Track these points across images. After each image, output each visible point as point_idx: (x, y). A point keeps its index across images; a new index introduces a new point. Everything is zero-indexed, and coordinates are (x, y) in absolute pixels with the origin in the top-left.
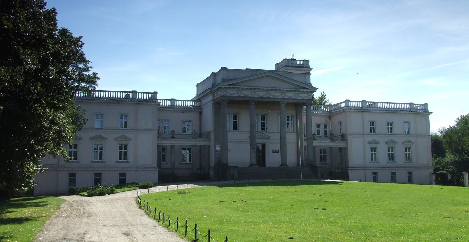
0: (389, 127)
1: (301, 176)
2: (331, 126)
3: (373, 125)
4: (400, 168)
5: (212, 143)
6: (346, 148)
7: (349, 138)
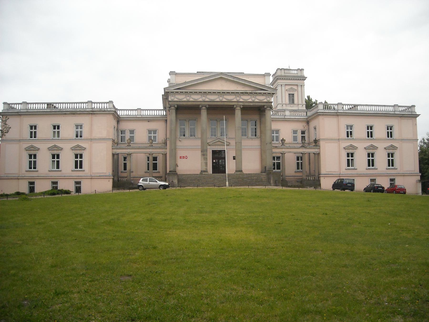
0: (389, 131)
1: (227, 183)
6: (319, 154)
7: (322, 143)
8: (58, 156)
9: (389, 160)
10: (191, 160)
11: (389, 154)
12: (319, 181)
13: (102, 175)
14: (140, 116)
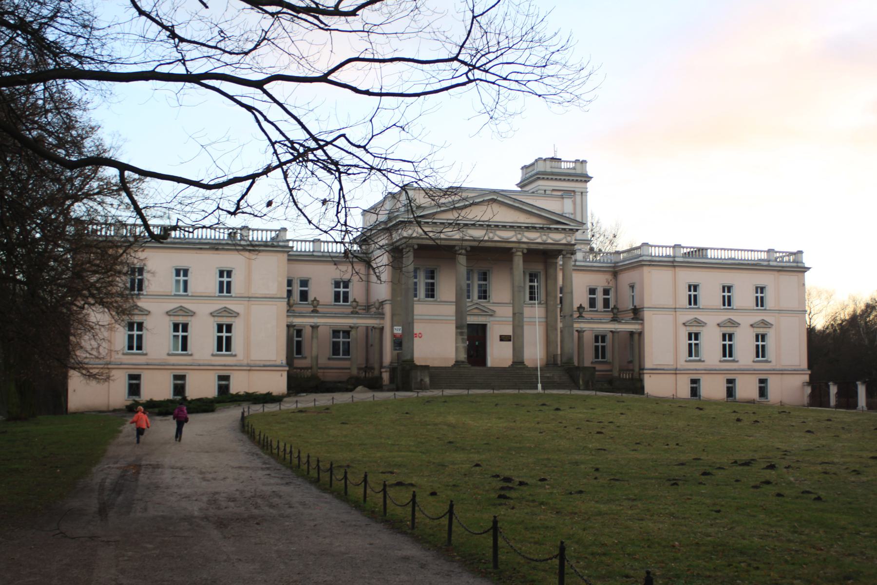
1: (540, 385)
2: (616, 291)
3: (695, 290)
4: (744, 372)
5: (387, 322)
6: (641, 334)
7: (647, 315)
8: (185, 328)
9: (724, 346)
10: (436, 342)
11: (757, 336)
12: (641, 381)
13: (268, 363)
14: (320, 254)
